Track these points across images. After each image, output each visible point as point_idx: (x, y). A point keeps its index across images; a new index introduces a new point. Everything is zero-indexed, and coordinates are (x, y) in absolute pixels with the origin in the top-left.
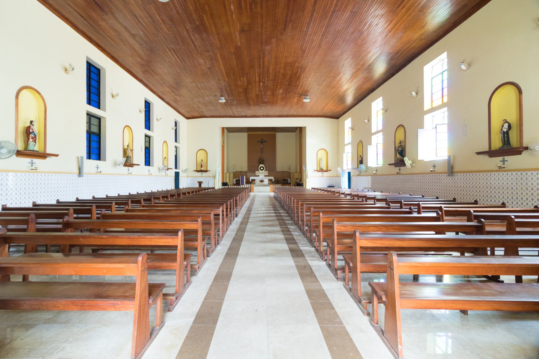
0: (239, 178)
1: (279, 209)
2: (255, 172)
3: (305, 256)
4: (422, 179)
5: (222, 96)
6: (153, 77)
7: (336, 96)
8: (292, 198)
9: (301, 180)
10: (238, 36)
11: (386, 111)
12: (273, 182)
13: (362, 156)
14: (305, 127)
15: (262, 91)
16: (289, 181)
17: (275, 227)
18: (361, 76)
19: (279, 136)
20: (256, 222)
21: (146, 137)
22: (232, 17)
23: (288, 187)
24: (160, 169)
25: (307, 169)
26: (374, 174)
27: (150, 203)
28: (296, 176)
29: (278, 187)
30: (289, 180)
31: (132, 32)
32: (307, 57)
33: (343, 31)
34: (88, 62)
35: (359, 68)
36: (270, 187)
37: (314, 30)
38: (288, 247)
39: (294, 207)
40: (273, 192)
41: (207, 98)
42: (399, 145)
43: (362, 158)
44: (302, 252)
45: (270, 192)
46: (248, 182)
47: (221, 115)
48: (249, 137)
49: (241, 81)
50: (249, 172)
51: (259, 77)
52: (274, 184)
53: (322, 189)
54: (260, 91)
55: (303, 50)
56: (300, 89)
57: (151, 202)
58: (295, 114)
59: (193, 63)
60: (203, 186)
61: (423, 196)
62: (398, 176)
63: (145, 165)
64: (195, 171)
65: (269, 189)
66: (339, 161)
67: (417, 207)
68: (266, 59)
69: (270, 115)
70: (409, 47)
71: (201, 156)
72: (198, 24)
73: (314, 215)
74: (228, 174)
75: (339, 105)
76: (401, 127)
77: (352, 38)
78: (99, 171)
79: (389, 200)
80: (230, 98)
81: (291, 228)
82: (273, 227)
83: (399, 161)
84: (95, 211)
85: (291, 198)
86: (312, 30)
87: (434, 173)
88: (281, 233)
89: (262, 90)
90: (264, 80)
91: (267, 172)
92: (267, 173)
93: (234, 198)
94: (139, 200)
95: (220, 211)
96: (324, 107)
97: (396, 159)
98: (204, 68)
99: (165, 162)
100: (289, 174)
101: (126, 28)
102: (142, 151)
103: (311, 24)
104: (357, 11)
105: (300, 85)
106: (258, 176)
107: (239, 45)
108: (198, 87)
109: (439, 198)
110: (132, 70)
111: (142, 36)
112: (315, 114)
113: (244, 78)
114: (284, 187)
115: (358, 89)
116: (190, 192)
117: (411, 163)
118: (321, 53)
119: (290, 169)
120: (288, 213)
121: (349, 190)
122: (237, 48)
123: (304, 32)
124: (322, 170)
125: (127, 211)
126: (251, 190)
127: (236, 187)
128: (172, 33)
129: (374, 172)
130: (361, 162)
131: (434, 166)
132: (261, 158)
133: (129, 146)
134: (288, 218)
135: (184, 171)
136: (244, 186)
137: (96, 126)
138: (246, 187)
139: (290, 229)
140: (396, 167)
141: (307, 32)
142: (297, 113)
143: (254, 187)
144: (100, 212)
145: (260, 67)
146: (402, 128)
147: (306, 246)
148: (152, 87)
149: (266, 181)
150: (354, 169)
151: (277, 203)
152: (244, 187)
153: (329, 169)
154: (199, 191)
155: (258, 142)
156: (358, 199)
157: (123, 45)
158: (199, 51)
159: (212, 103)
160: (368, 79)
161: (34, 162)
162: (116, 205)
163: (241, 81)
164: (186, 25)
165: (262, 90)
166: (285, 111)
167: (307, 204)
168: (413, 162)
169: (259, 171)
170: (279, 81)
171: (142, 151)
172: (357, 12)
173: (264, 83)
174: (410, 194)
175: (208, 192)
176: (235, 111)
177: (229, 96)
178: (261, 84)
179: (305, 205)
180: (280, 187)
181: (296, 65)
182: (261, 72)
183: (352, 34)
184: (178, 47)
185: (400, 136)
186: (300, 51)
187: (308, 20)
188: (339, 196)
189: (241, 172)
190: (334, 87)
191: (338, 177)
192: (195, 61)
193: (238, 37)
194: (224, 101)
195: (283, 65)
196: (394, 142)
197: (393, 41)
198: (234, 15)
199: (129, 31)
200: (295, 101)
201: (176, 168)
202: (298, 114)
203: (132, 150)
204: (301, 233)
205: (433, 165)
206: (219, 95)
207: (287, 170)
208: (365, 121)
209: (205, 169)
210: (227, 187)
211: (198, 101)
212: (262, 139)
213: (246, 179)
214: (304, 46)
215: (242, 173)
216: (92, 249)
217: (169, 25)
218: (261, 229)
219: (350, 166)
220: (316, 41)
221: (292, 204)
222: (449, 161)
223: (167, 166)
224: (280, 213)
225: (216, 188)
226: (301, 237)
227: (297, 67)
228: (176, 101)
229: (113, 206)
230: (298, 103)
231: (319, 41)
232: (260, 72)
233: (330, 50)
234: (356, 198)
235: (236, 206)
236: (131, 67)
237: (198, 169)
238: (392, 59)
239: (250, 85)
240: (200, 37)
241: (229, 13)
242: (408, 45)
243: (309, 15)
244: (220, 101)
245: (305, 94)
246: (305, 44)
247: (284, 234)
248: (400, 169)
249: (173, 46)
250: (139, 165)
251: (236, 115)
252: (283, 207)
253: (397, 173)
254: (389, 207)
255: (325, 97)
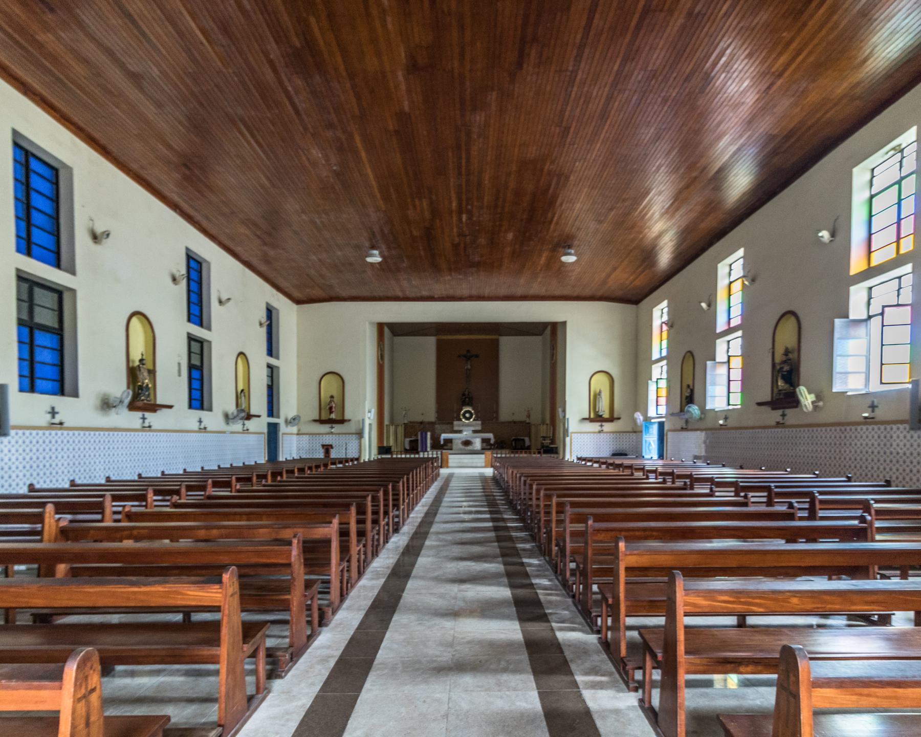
0: (416, 435)
1: (502, 508)
2: (452, 423)
3: (573, 667)
4: (840, 437)
5: (373, 247)
6: (203, 195)
7: (634, 248)
8: (534, 487)
9: (553, 441)
10: (403, 84)
11: (753, 280)
12: (491, 445)
13: (691, 387)
14: (564, 324)
15: (466, 236)
16: (527, 443)
17: (490, 562)
18: (697, 200)
19: (506, 343)
20: (444, 546)
21: (193, 343)
22: (384, 25)
23: (525, 455)
24: (231, 417)
25: (567, 416)
26: (721, 425)
27: (99, 517)
28: (543, 430)
29: (503, 456)
30: (527, 439)
31: (128, 66)
32: (574, 144)
33: (664, 73)
34: (16, 145)
35: (696, 178)
36: (486, 457)
37: (592, 70)
38: (523, 631)
39: (538, 506)
40: (492, 466)
41: (339, 253)
42: (784, 358)
43: (692, 391)
44: (562, 652)
45: (486, 467)
46: (436, 445)
47: (375, 294)
48: (441, 348)
49: (415, 207)
50: (439, 424)
51: (460, 200)
52: (493, 449)
53: (594, 460)
54: (461, 235)
55: (564, 124)
56: (555, 231)
57: (103, 513)
58: (543, 292)
59: (296, 159)
60: (334, 454)
61: (848, 477)
62: (780, 430)
63: (191, 407)
64: (315, 421)
65: (483, 460)
66: (638, 400)
67: (808, 500)
68: (474, 153)
69: (486, 295)
70: (819, 119)
71: (330, 387)
72: (298, 44)
73: (595, 538)
74: (392, 429)
75: (643, 272)
76: (788, 315)
77: (685, 93)
78: (56, 420)
79: (776, 490)
80: (394, 252)
81: (530, 565)
82: (485, 562)
83: (782, 396)
84: (110, 506)
85: (531, 486)
86: (587, 67)
87: (724, 429)
88: (505, 580)
89: (467, 233)
90: (469, 207)
91: (479, 422)
92: (478, 425)
93: (390, 487)
94: (226, 481)
95: (331, 530)
96: (609, 276)
97: (775, 390)
98: (324, 173)
99: (243, 401)
100: (526, 426)
101: (108, 52)
102: (180, 375)
103: (587, 51)
104: (704, 11)
105: (555, 219)
106: (460, 432)
107: (406, 108)
108: (314, 223)
109: (893, 484)
110: (149, 178)
111: (158, 79)
112: (587, 292)
113: (424, 200)
114: (517, 455)
115: (685, 234)
116: (303, 466)
117: (814, 399)
118: (608, 135)
119: (529, 416)
120: (522, 520)
121: (661, 462)
122: (402, 118)
123: (569, 73)
124: (598, 418)
125: (176, 505)
126: (444, 464)
127: (408, 456)
128: (234, 73)
129: (721, 422)
130: (690, 400)
131: (873, 407)
132: (466, 393)
133: (144, 362)
134: (522, 534)
135: (290, 422)
136: (426, 453)
137: (50, 311)
138: (430, 456)
139: (528, 569)
140: (773, 409)
141: (575, 72)
142: (546, 291)
143: (450, 456)
144: (120, 509)
145: (460, 174)
146: (793, 319)
147: (573, 630)
148: (205, 223)
149: (477, 444)
150: (673, 414)
151: (497, 494)
152: (426, 456)
153: (615, 416)
154: (310, 468)
155: (459, 356)
156: (673, 482)
157: (114, 107)
158: (309, 126)
159: (351, 264)
160: (712, 205)
161: (146, 416)
162: (155, 494)
163: (415, 207)
164: (269, 47)
165: (467, 233)
166: (521, 285)
167: (574, 505)
168: (819, 398)
169: (461, 420)
170: (506, 210)
171: (180, 375)
172: (705, 14)
173: (470, 213)
174: (815, 474)
175: (353, 464)
176: (405, 283)
177: (389, 248)
178: (464, 217)
179: (568, 509)
180: (508, 455)
181: (546, 167)
182: (464, 186)
183: (685, 80)
184: (253, 113)
185: (786, 337)
186: (558, 129)
187: (579, 37)
188: (632, 474)
189: (421, 423)
190: (632, 227)
191: (635, 432)
192: (301, 153)
193: (403, 87)
194: (379, 259)
195: (514, 168)
196: (771, 351)
197: (784, 104)
198: (389, 19)
199: (122, 66)
200: (543, 260)
201: (271, 413)
202: (549, 293)
203: (152, 372)
204: (557, 582)
205: (870, 403)
206: (367, 245)
207: (522, 417)
208: (701, 306)
209: (339, 418)
210: (389, 456)
211: (320, 260)
212: (468, 351)
213: (432, 438)
214: (567, 113)
215: (424, 426)
216: (32, 615)
217: (223, 46)
218: (453, 568)
219: (663, 410)
220: (598, 100)
221: (534, 499)
222: (914, 393)
223: (247, 410)
224: (504, 520)
225: (365, 457)
226: (557, 595)
227: (549, 172)
228: (267, 260)
229: (47, 515)
230: (548, 266)
231: (603, 100)
232: (460, 186)
233: (629, 129)
234: (669, 479)
235: (396, 506)
236: (142, 168)
237: (323, 418)
238: (774, 153)
239: (438, 221)
240: (305, 84)
241: (375, 12)
242: (818, 116)
243: (583, 23)
244: (369, 260)
245: (565, 243)
246: (569, 108)
247: (512, 586)
248: (783, 415)
249: (240, 111)
250: (170, 407)
251: (408, 293)
252: (511, 504)
253: (778, 423)
254: (791, 511)
255: (611, 251)
